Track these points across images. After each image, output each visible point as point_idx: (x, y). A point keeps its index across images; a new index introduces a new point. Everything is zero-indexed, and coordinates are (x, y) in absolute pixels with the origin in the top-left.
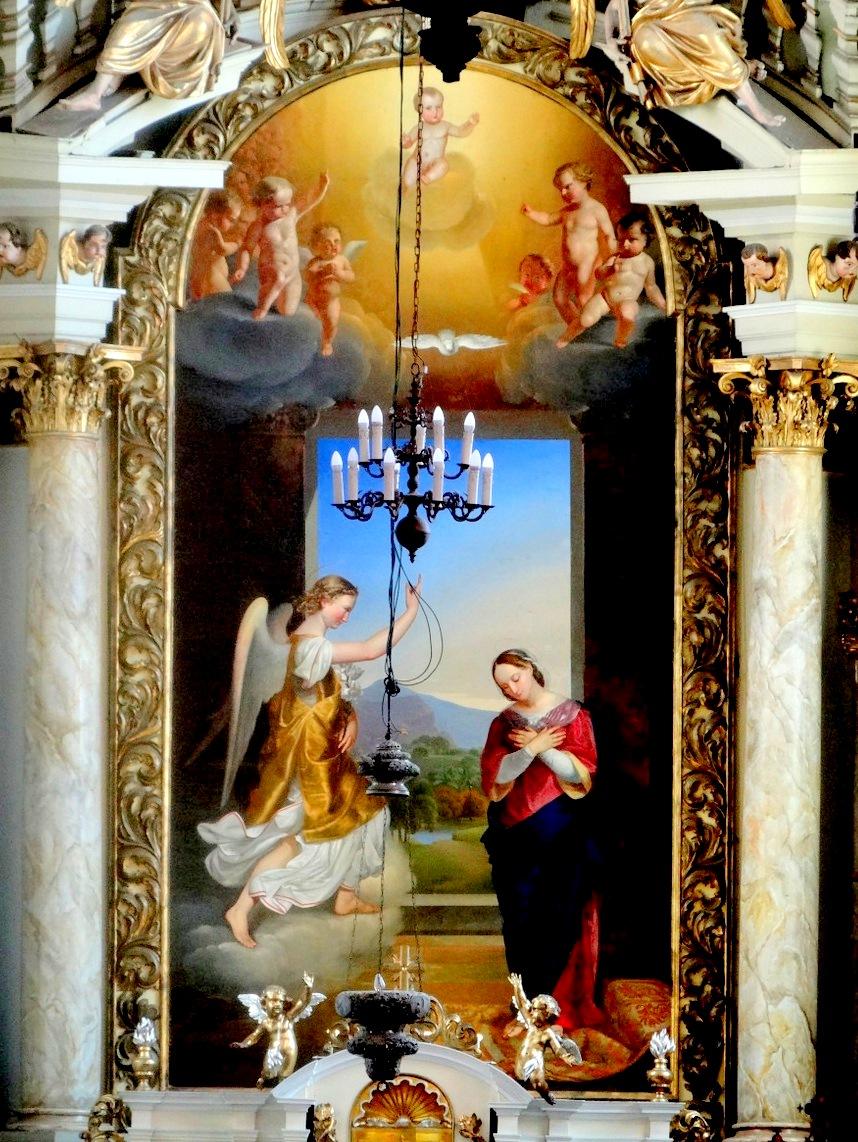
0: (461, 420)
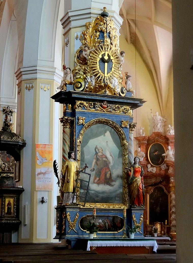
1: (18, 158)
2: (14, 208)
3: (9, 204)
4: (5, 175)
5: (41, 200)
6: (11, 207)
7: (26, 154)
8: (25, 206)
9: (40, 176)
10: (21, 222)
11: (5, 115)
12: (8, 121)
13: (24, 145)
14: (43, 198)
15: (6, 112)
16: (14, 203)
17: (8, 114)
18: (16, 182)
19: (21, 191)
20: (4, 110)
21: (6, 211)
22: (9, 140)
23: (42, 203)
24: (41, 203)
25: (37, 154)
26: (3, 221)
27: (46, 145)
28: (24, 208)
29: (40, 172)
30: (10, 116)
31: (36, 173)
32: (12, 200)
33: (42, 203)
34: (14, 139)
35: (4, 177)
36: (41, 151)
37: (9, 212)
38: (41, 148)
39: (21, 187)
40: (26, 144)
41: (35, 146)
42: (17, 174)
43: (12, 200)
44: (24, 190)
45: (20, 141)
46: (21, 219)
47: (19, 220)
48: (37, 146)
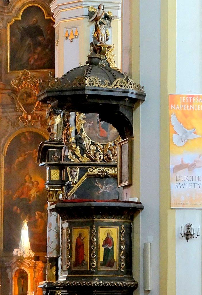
0: (69, 116)
1: (126, 129)
2: (120, 250)
3: (108, 241)
4: (96, 171)
5: (184, 230)
6: (113, 248)
7: (143, 119)
8: (145, 246)
9: (180, 173)
10: (136, 286)
11: (93, 25)
12: (100, 41)
13: (136, 101)
14: (189, 227)
15: (96, 19)
16: (119, 238)
17: (101, 23)
18: (124, 187)
19: (130, 212)
20: (91, 14)
21: (101, 259)
22: (104, 87)
23: (187, 239)
24: (184, 238)
25: (174, 121)
26: (96, 283)
27: (193, 96)
28: (145, 251)
29: (181, 163)
30: (105, 29)
31: (172, 166)
32: (114, 232)
33: (187, 239)
34: (117, 83)
35: (96, 176)
36: (183, 111)
37: (108, 262)
38: (183, 104)
39: (137, 201)
40: (145, 96)
41: (167, 101)
42: (126, 169)
43: (114, 232)
44: (142, 209)
45: (131, 90)
46: (138, 275)
47: (131, 279)
48: (173, 99)
